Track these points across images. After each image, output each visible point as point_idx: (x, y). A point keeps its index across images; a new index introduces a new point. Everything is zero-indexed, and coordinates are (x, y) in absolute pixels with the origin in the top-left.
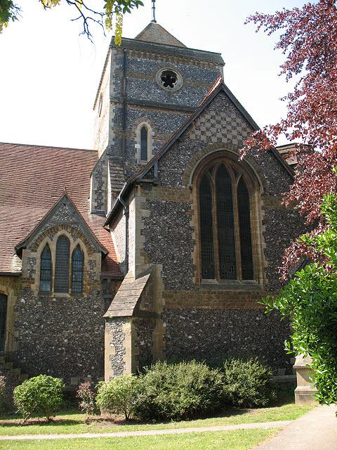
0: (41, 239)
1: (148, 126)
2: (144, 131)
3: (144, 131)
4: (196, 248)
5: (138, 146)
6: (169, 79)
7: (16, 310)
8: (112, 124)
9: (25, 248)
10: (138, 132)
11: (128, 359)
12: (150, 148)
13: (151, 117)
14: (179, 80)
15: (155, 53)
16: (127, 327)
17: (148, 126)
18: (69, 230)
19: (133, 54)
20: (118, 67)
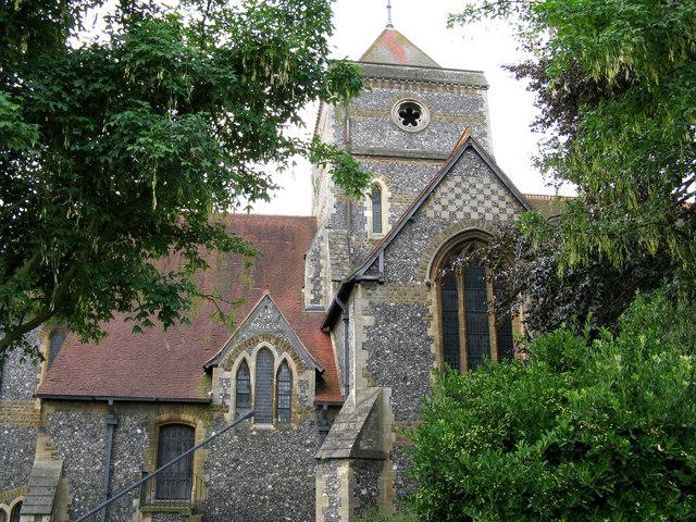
1: (383, 184)
5: (369, 214)
12: (386, 215)
14: (425, 116)
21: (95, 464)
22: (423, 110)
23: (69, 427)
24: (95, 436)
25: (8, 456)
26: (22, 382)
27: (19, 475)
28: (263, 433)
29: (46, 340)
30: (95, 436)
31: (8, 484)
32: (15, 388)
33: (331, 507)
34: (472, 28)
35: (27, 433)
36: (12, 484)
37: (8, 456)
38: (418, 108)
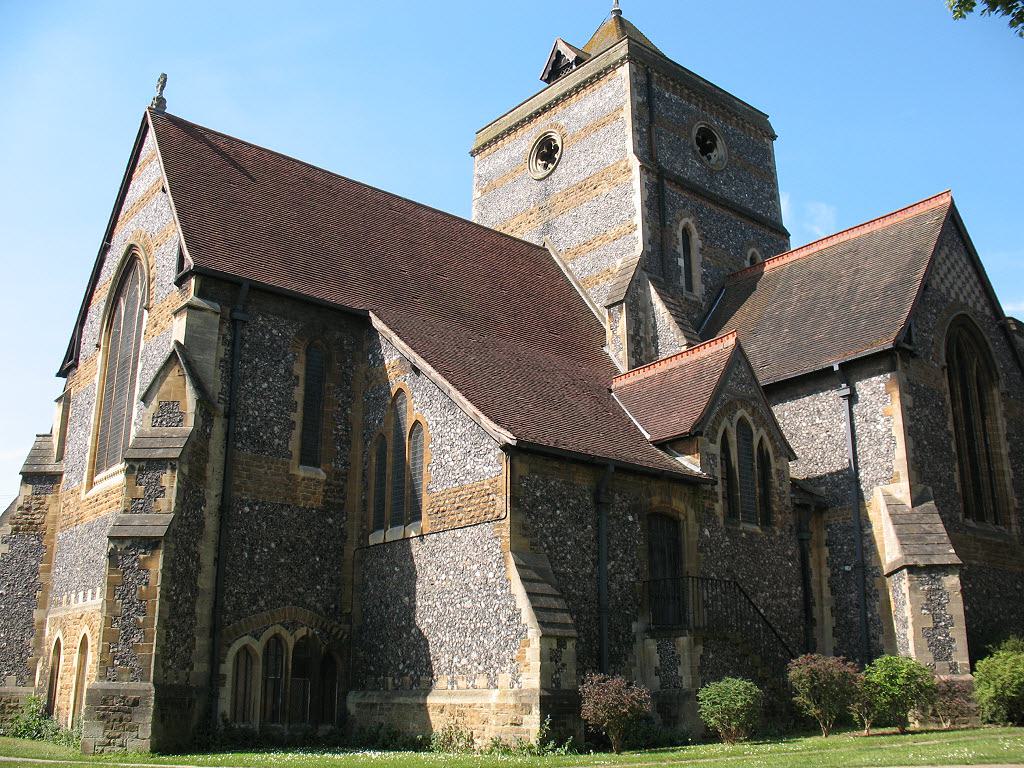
0: (717, 421)
1: (693, 227)
2: (686, 233)
3: (686, 233)
4: (297, 432)
5: (681, 262)
6: (706, 142)
7: (700, 549)
8: (646, 210)
9: (701, 434)
10: (680, 235)
11: (959, 635)
12: (697, 272)
13: (696, 212)
14: (720, 151)
15: (688, 89)
16: (952, 581)
17: (693, 227)
18: (750, 410)
19: (659, 81)
20: (640, 100)
21: (585, 564)
22: (720, 143)
23: (548, 501)
24: (581, 520)
25: (252, 552)
26: (268, 424)
27: (271, 586)
28: (751, 535)
29: (303, 357)
30: (581, 520)
31: (255, 602)
32: (257, 431)
33: (936, 628)
34: (155, 82)
35: (281, 516)
36: (262, 603)
37: (252, 552)
38: (714, 139)
